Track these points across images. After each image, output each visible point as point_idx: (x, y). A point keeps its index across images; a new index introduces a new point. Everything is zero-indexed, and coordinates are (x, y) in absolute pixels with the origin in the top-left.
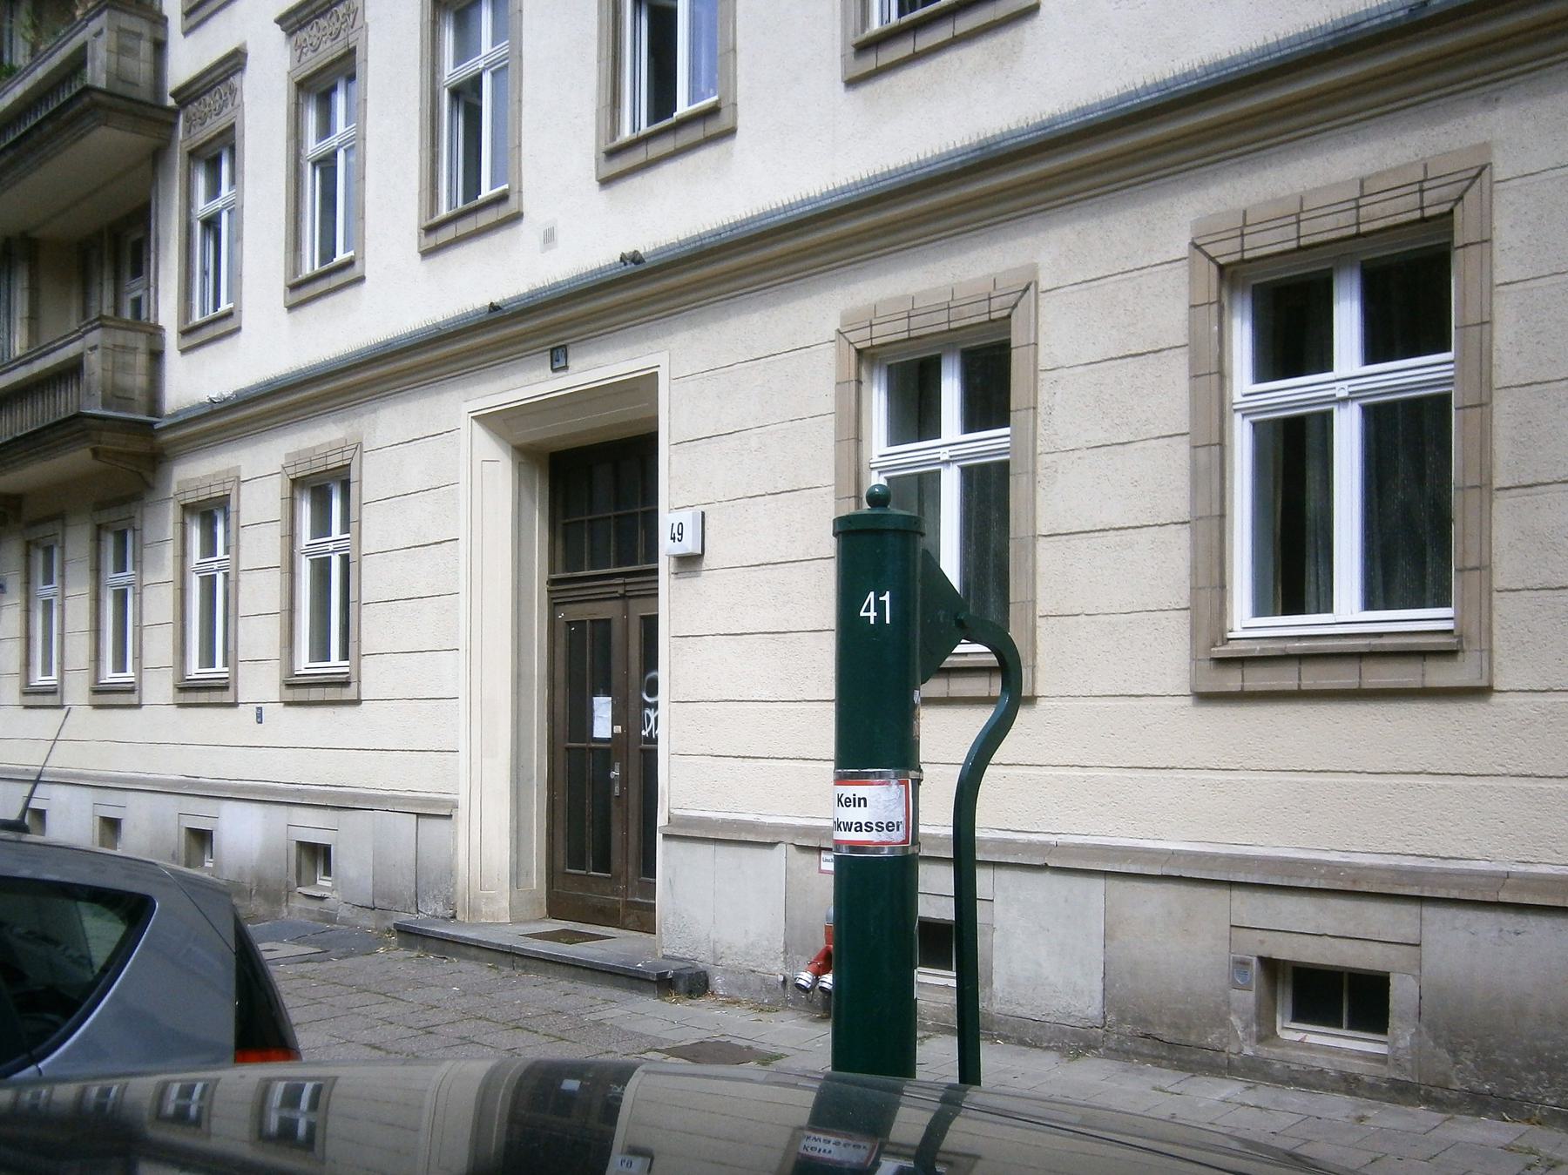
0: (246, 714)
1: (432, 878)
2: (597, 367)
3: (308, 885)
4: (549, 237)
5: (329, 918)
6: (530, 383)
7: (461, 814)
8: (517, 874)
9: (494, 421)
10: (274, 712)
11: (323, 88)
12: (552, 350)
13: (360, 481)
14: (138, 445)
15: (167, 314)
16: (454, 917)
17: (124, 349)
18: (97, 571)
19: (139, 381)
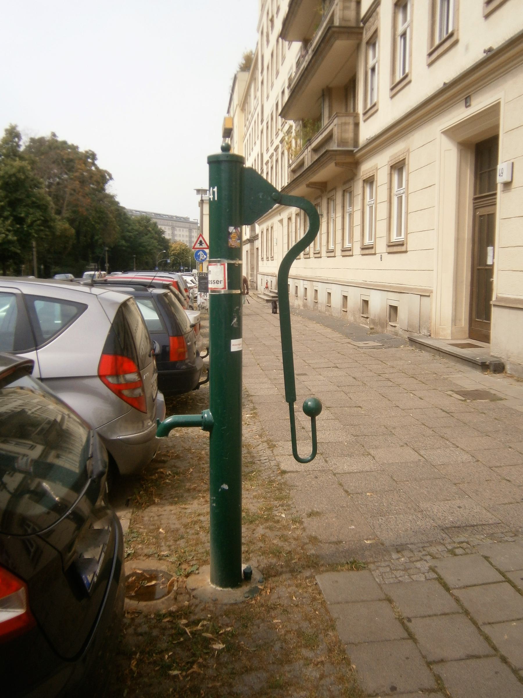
0: (378, 256)
1: (423, 321)
2: (481, 103)
3: (393, 321)
4: (467, 48)
5: (396, 334)
6: (459, 114)
7: (434, 295)
8: (455, 320)
9: (450, 133)
10: (386, 256)
11: (403, 4)
12: (466, 98)
13: (408, 164)
14: (349, 160)
15: (360, 109)
16: (430, 336)
17: (345, 124)
18: (343, 207)
19: (350, 135)
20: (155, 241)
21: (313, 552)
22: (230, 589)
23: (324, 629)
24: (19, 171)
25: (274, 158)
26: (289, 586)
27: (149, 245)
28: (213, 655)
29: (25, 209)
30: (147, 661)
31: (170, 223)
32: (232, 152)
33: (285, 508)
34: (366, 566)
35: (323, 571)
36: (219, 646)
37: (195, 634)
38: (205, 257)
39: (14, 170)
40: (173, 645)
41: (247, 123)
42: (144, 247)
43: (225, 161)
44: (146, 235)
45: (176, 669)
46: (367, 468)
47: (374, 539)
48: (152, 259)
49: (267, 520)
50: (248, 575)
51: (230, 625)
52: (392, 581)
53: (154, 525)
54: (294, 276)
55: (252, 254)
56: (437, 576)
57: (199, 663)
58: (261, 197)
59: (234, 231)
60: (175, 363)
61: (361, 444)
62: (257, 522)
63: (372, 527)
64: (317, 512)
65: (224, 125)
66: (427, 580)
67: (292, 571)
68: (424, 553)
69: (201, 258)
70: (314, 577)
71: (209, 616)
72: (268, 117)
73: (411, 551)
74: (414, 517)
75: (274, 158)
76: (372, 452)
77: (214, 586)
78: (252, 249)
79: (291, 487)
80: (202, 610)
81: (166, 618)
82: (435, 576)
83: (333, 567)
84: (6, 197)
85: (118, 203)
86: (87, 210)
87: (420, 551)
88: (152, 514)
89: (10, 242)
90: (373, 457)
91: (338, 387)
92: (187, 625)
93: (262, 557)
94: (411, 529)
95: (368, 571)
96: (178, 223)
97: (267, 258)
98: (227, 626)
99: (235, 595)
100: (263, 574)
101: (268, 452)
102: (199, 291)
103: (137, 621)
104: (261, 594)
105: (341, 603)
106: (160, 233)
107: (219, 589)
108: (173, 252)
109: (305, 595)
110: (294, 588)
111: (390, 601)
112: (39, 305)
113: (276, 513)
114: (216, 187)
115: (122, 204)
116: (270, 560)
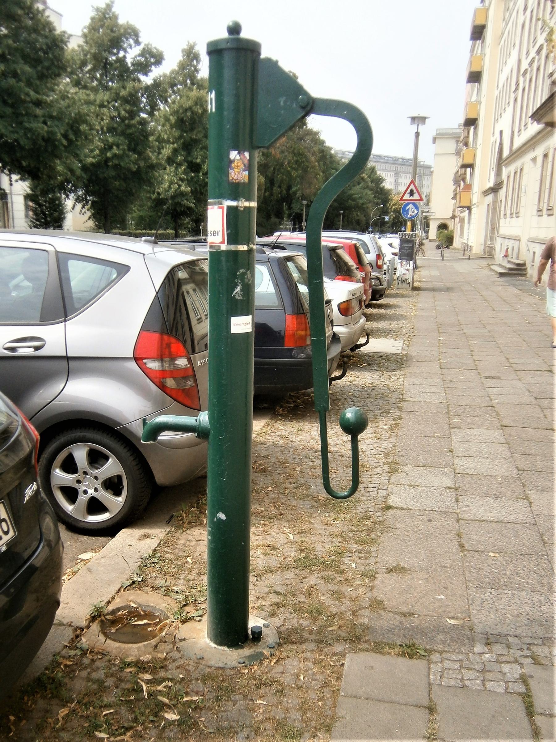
20: (370, 193)
21: (366, 621)
22: (226, 648)
23: (315, 728)
24: (196, 104)
25: (535, 65)
26: (306, 660)
27: (361, 198)
28: (159, 726)
29: (202, 153)
30: (80, 714)
31: (394, 167)
32: (244, 35)
33: (362, 555)
34: (426, 654)
35: (360, 650)
36: (172, 716)
37: (151, 695)
38: (416, 212)
39: (190, 103)
40: (119, 702)
41: (507, 14)
42: (354, 200)
43: (228, 49)
44: (359, 184)
45: (104, 731)
46: (512, 518)
47: (463, 619)
48: (365, 216)
49: (328, 567)
50: (257, 636)
51: (202, 693)
52: (452, 683)
53: (185, 551)
54: (543, 240)
55: (494, 209)
56: (524, 691)
57: (137, 730)
58: (282, 103)
59: (238, 157)
60: (291, 350)
61: (522, 483)
62: (314, 568)
63: (470, 602)
64: (403, 568)
65: (474, 21)
66: (507, 692)
67: (320, 642)
68: (527, 653)
69: (410, 213)
70: (344, 656)
71: (181, 676)
72: (534, 2)
73: (508, 647)
74: (542, 599)
75: (535, 65)
76: (533, 496)
77: (208, 641)
78: (495, 202)
79: (387, 528)
80: (178, 667)
81: (131, 667)
82: (523, 689)
83: (378, 648)
84: (181, 137)
85: (323, 142)
86: (282, 152)
87: (521, 649)
88: (191, 538)
89: (182, 194)
90: (530, 503)
91: (536, 398)
92: (148, 682)
93: (293, 615)
94: (528, 614)
95: (426, 662)
96: (404, 167)
97: (511, 214)
98: (197, 693)
99: (231, 656)
100: (280, 637)
101: (384, 478)
102: (399, 259)
103: (98, 664)
104: (261, 663)
105: (360, 698)
106: (379, 181)
107: (213, 645)
108: (394, 208)
109: (319, 676)
110: (310, 664)
111: (431, 710)
112: (73, 266)
113: (346, 560)
114: (214, 92)
115: (328, 144)
116: (302, 622)
